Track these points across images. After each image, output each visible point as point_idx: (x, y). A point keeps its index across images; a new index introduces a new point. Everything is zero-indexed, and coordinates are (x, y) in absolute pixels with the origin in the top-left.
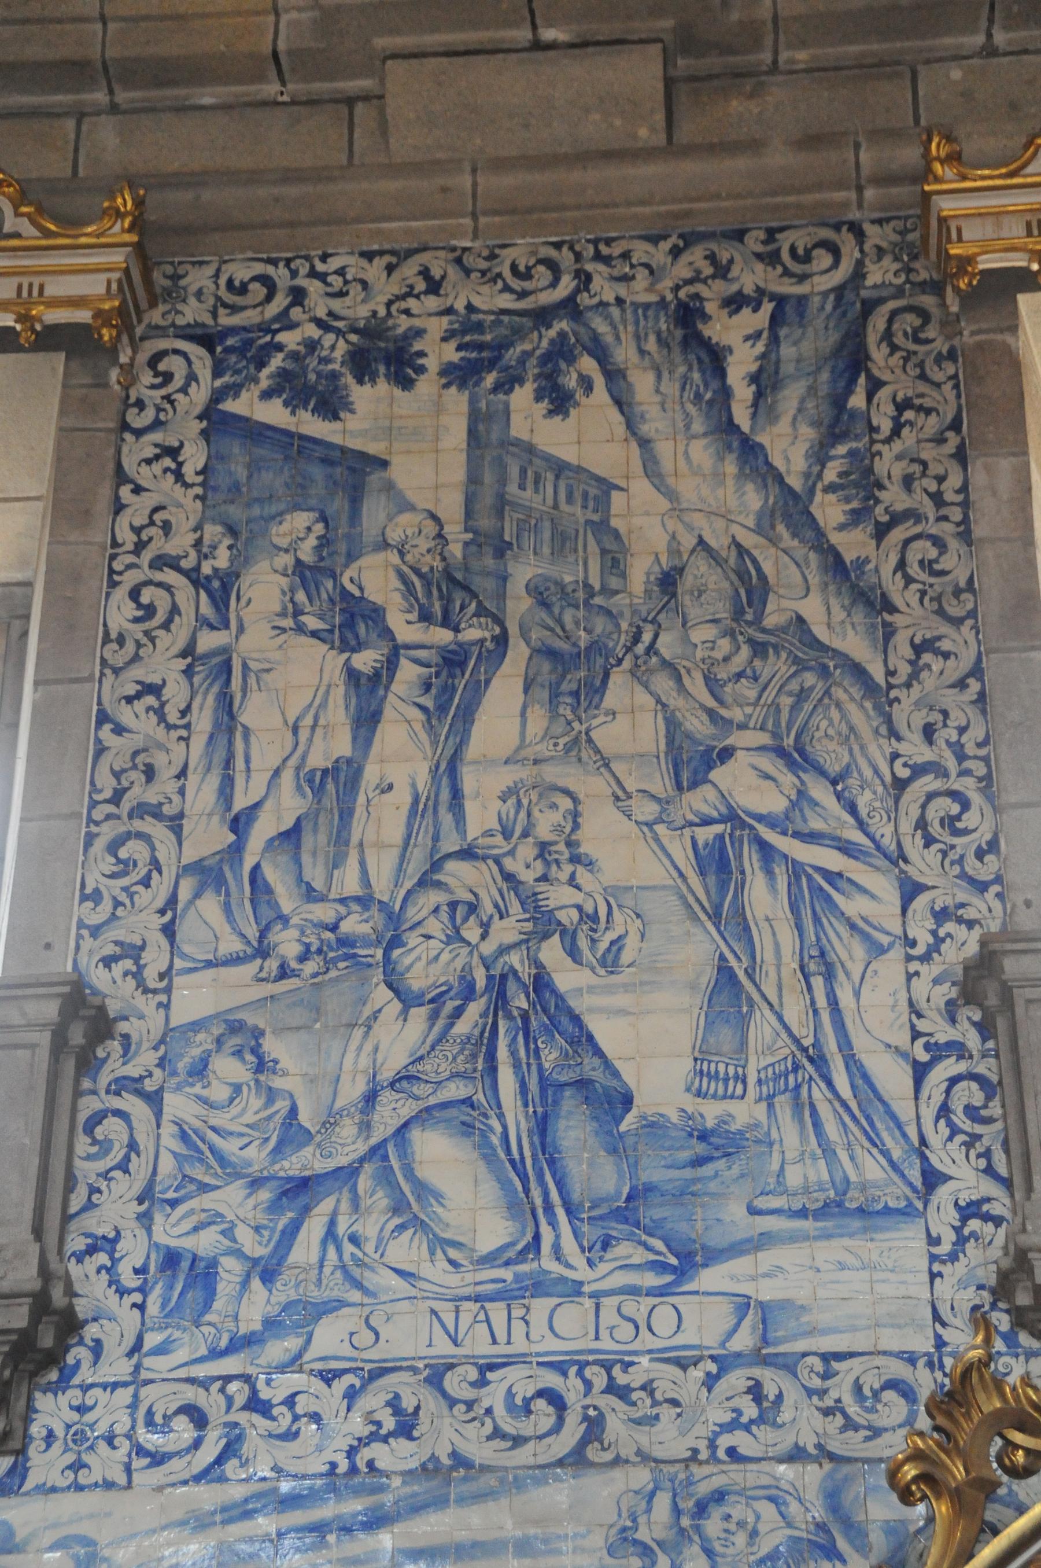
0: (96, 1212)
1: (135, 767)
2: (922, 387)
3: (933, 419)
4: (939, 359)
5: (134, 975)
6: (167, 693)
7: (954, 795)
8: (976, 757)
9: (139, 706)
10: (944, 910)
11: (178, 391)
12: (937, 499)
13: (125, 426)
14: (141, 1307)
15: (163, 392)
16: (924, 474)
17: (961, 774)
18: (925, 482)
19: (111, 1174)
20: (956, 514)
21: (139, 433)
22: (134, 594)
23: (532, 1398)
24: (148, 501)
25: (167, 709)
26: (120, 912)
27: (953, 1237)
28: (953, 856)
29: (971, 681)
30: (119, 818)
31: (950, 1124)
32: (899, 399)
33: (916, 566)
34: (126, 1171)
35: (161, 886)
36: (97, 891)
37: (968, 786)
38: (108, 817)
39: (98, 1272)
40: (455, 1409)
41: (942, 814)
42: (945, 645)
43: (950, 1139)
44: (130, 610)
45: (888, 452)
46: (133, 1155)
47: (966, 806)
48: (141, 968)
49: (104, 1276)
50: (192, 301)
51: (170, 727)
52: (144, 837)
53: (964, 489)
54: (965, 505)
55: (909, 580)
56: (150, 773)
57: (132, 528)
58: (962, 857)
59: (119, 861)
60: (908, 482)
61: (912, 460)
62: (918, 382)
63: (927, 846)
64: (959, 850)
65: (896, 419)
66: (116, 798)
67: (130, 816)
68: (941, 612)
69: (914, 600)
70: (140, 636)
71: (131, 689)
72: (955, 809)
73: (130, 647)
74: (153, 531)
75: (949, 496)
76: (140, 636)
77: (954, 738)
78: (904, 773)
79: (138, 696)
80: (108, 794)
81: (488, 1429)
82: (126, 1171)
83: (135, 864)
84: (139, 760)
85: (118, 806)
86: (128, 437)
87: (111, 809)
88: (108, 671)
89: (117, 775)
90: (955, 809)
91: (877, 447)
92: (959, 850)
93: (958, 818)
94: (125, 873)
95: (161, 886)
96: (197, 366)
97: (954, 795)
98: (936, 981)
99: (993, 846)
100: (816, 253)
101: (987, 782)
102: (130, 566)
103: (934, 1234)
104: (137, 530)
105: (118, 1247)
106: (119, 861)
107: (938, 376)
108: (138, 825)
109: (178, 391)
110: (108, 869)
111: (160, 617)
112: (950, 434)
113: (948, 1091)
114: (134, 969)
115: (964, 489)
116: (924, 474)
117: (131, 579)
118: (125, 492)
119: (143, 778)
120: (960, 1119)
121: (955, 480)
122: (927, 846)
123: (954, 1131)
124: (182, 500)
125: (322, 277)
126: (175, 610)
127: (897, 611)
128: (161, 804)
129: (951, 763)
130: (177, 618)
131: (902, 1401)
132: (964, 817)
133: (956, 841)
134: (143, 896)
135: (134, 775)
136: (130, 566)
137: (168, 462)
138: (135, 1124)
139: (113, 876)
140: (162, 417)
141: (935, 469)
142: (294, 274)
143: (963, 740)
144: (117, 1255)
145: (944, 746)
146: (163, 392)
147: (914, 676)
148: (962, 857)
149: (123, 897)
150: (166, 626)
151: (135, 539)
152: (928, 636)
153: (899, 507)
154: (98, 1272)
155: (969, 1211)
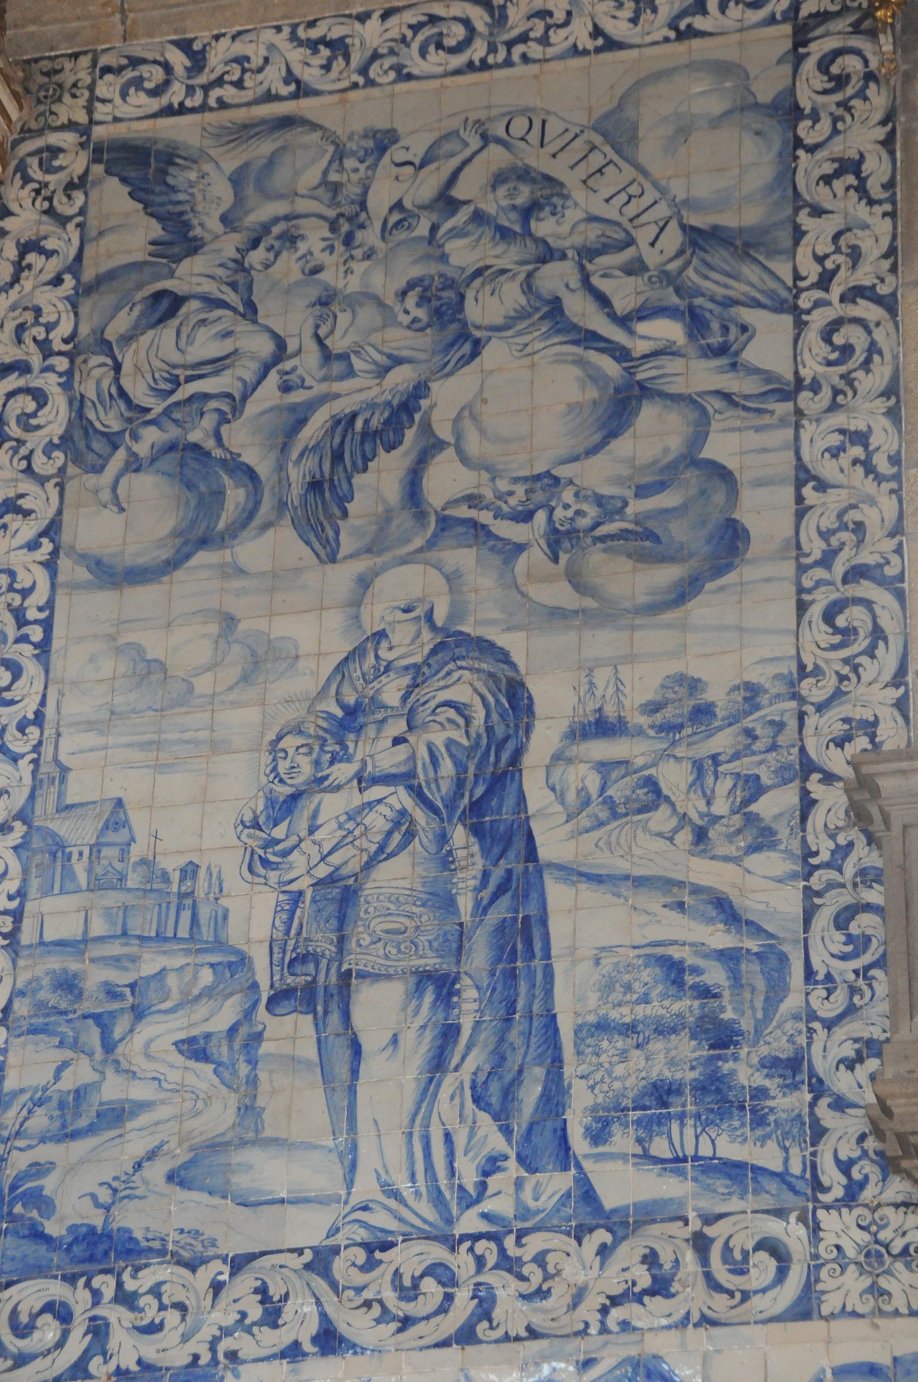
2: (27, 486)
5: (857, 189)
6: (867, 168)
9: (839, 185)
12: (44, 346)
13: (798, 143)
14: (892, 215)
15: (842, 369)
17: (17, 641)
21: (829, 1025)
24: (835, 500)
25: (869, 184)
26: (840, 398)
28: (23, 451)
29: (67, 277)
30: (843, 886)
33: (13, 423)
36: (829, 977)
37: (50, 383)
42: (49, 244)
48: (862, 181)
50: (67, 98)
53: (50, 605)
54: (47, 625)
56: (855, 255)
57: (820, 533)
58: (32, 452)
61: (26, 309)
62: (45, 218)
64: (29, 445)
68: (50, 212)
70: (836, 380)
73: (826, 394)
75: (58, 345)
76: (836, 380)
77: (41, 337)
80: (813, 278)
84: (842, 242)
85: (827, 290)
86: (800, 153)
87: (818, 294)
88: (816, 1025)
89: (820, 259)
92: (29, 445)
93: (34, 415)
94: (855, 955)
97: (27, 391)
99: (39, 718)
101: (44, 648)
102: (817, 304)
104: (825, 535)
105: (864, 167)
110: (836, 949)
111: (859, 356)
114: (855, 183)
115: (50, 605)
118: (803, 218)
121: (40, 596)
124: (869, 220)
126: (873, 349)
128: (874, 286)
129: (36, 360)
130: (876, 358)
132: (40, 414)
133: (49, 178)
134: (869, 669)
135: (844, 536)
136: (817, 304)
137: (857, 451)
139: (844, 957)
141: (23, 580)
143: (51, 337)
145: (32, 344)
146: (842, 369)
148: (32, 452)
149: (841, 385)
151: (819, 269)
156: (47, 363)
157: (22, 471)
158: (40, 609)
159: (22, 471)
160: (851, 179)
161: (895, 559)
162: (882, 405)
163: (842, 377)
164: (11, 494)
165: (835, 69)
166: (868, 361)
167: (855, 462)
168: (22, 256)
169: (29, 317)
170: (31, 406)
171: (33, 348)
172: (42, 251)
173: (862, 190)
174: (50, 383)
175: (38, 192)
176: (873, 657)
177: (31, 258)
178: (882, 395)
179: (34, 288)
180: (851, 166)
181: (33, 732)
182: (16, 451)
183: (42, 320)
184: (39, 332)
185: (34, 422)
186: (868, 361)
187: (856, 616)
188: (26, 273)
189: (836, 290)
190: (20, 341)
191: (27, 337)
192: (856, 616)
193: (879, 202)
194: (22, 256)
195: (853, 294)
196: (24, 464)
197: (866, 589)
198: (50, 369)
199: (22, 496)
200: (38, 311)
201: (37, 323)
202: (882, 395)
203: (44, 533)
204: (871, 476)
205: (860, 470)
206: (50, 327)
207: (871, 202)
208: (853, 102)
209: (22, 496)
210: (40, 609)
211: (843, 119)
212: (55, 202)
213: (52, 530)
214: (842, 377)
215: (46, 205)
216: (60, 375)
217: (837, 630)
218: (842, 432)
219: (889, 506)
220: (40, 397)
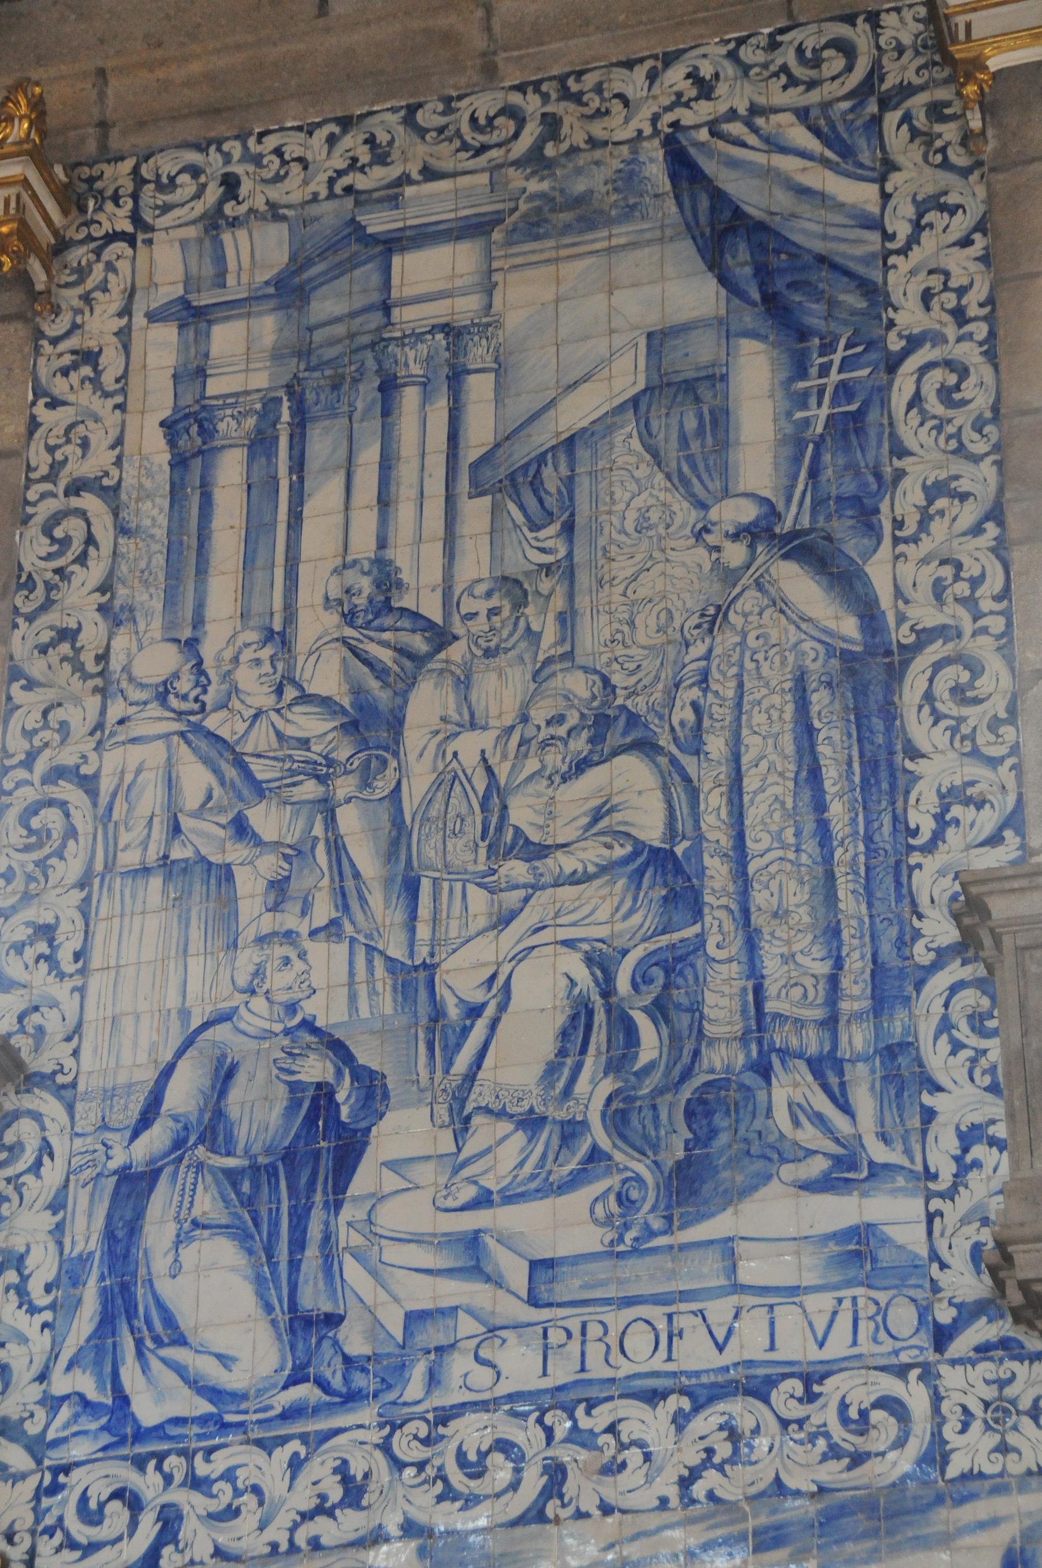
0: (57, 607)
1: (46, 726)
2: (958, 466)
3: (970, 505)
4: (995, 723)
7: (949, 364)
8: (992, 613)
10: (937, 484)
11: (74, 562)
12: (959, 315)
15: (36, 855)
16: (957, 578)
17: (959, 340)
18: (945, 296)
19: (49, 862)
20: (981, 330)
22: (47, 530)
23: (495, 117)
27: (953, 1168)
29: (1008, 834)
31: (922, 412)
32: (929, 483)
34: (62, 858)
35: (53, 1174)
37: (970, 353)
38: (43, 496)
39: (37, 961)
40: (428, 137)
41: (970, 1011)
43: (922, 424)
44: (44, 546)
45: (931, 864)
46: (46, 1159)
47: (963, 372)
49: (43, 966)
51: (106, 395)
52: (82, 514)
55: (937, 717)
56: (85, 444)
59: (31, 832)
60: (938, 589)
63: (953, 1053)
65: (940, 818)
66: (51, 477)
67: (67, 494)
69: (962, 1075)
71: (46, 636)
72: (952, 379)
74: (68, 449)
75: (973, 311)
77: (952, 304)
78: (945, 1315)
79: (53, 644)
80: (44, 470)
81: (457, 143)
82: (62, 858)
83: (49, 836)
90: (952, 379)
91: (914, 859)
92: (972, 722)
93: (957, 388)
95: (53, 1174)
96: (77, 819)
97: (949, 364)
98: (924, 561)
100: (826, 54)
103: (933, 1170)
106: (31, 832)
107: (980, 447)
108: (75, 502)
109: (74, 562)
110: (20, 843)
112: (977, 237)
113: (919, 381)
114: (47, 951)
116: (957, 578)
117: (44, 510)
119: (79, 452)
120: (964, 1032)
121: (995, 582)
122: (953, 1053)
123: (957, 1046)
124: (101, 413)
125: (257, 160)
126: (46, 1149)
127: (940, 1089)
131: (892, 1420)
133: (965, 711)
135: (46, 735)
138: (92, 520)
140: (79, 320)
141: (971, 569)
142: (227, 158)
144: (27, 1272)
147: (913, 240)
150: (82, 559)
152: (958, 782)
153: (929, 623)
154: (37, 961)
155: (969, 1137)
156: (981, 623)
157: (985, 1089)
158: (981, 305)
159: (985, 1089)
160: (43, 947)
161: (115, 472)
162: (49, 1220)
163: (80, 297)
164: (943, 475)
165: (58, 533)
166: (38, 1164)
167: (64, 659)
168: (920, 216)
169: (947, 572)
170: (965, 676)
171: (947, 318)
172: (943, 208)
173: (95, 382)
174: (970, 353)
175: (954, 730)
176: (38, 1176)
177: (941, 503)
178: (97, 590)
179: (939, 249)
180: (89, 357)
181: (1008, 732)
182: (939, 428)
183: (963, 574)
184: (962, 588)
185: (957, 396)
186: (38, 1164)
187: (73, 527)
188: (973, 1176)
189: (41, 766)
190: (928, 309)
191: (935, 303)
192: (73, 527)
193: (92, 676)
194: (920, 216)
195: (57, 774)
196: (939, 158)
197: (89, 501)
198: (984, 631)
199: (957, 478)
200: (959, 566)
201: (946, 288)
202: (97, 590)
203: (987, 518)
204: (298, 1518)
205: (67, 667)
206: (961, 291)
207: (61, 976)
208: (94, 295)
209: (957, 478)
210: (981, 305)
211: (82, 313)
212: (980, 740)
213: (996, 514)
214: (80, 297)
215: (953, 444)
216: (981, 344)
217: (53, 540)
218: (74, 352)
219: (70, 1006)
220: (975, 669)
